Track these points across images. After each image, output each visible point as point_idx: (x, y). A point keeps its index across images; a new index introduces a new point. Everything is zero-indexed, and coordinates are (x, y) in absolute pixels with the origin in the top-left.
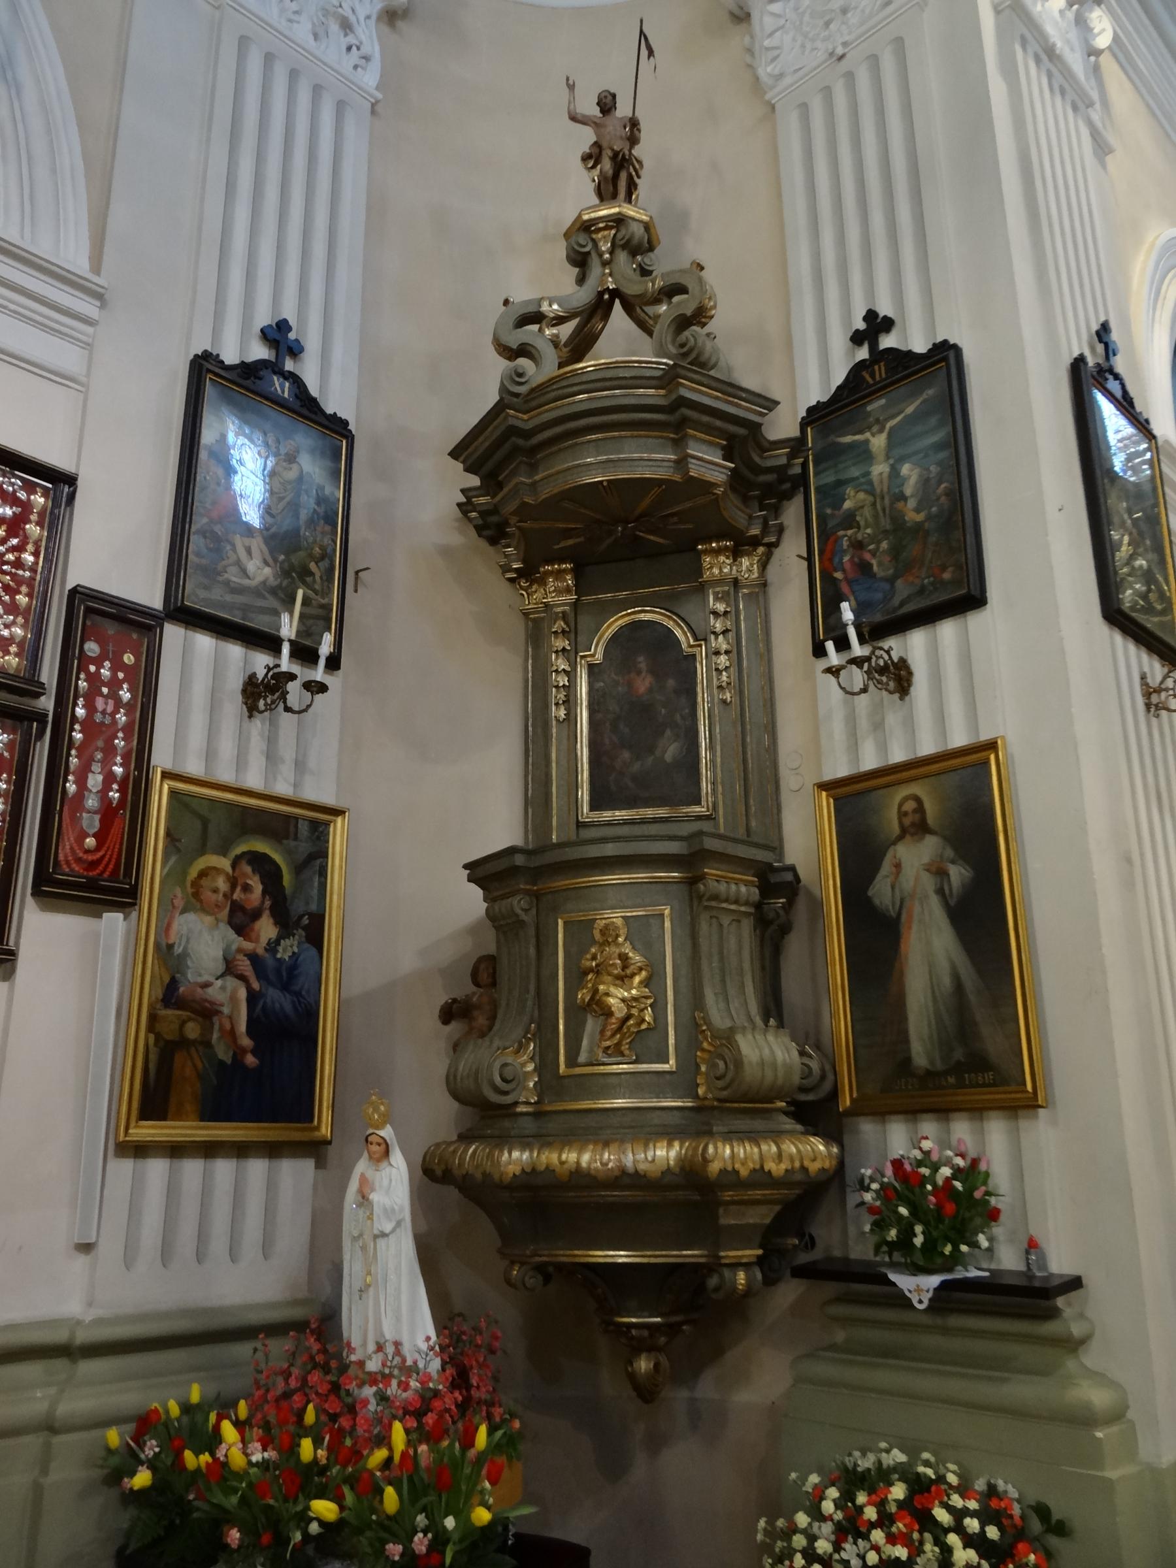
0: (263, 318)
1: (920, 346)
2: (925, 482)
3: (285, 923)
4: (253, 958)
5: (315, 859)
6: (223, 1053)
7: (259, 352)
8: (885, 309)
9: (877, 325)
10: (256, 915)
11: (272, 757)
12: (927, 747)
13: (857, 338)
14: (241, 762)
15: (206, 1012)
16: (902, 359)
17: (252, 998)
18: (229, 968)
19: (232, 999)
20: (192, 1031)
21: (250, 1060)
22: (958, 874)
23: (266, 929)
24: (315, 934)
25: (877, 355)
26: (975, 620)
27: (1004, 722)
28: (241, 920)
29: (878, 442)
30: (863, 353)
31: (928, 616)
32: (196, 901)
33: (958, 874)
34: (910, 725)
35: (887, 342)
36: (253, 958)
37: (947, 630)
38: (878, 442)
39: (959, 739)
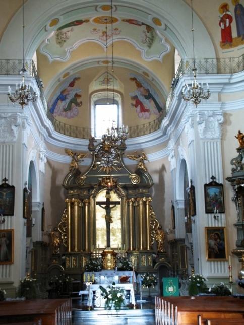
0: (211, 177)
1: (10, 184)
2: (9, 201)
3: (220, 240)
4: (217, 243)
5: (223, 232)
6: (216, 253)
7: (211, 180)
8: (7, 178)
9: (5, 180)
10: (217, 239)
11: (218, 223)
12: (6, 228)
13: (3, 180)
14: (215, 224)
15: (213, 249)
16: (8, 185)
17: (218, 247)
18: (215, 245)
19: (216, 248)
20: (212, 251)
21: (219, 253)
22: (8, 242)
23: (218, 240)
24: (224, 240)
25: (5, 184)
26: (12, 217)
27: (14, 228)
28: (216, 240)
29: (5, 194)
30: (3, 182)
31: (8, 215)
32: (211, 239)
33: (8, 242)
34: (4, 225)
35: (7, 182)
36: (217, 243)
37: (9, 217)
38: (5, 194)
39: (9, 228)
